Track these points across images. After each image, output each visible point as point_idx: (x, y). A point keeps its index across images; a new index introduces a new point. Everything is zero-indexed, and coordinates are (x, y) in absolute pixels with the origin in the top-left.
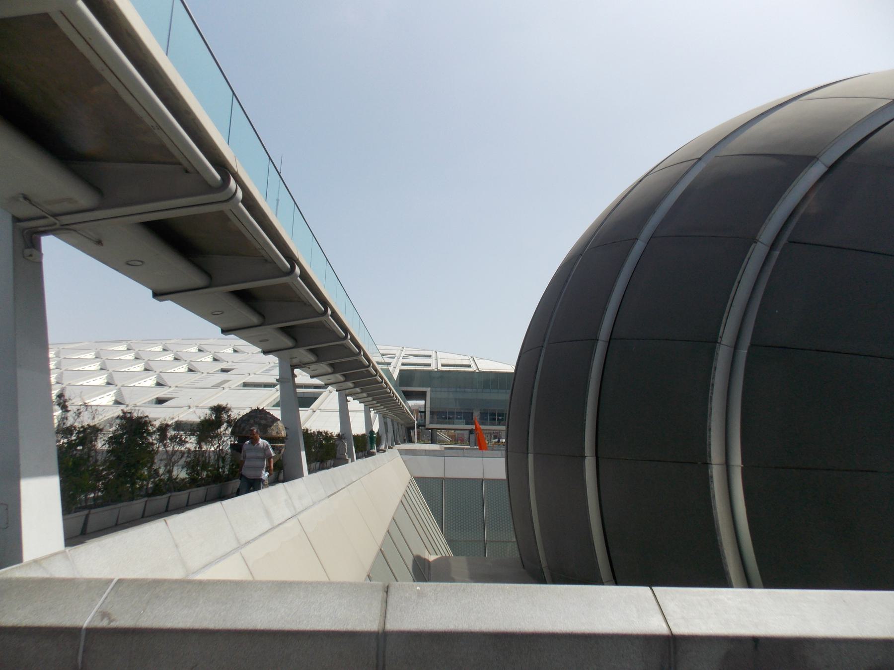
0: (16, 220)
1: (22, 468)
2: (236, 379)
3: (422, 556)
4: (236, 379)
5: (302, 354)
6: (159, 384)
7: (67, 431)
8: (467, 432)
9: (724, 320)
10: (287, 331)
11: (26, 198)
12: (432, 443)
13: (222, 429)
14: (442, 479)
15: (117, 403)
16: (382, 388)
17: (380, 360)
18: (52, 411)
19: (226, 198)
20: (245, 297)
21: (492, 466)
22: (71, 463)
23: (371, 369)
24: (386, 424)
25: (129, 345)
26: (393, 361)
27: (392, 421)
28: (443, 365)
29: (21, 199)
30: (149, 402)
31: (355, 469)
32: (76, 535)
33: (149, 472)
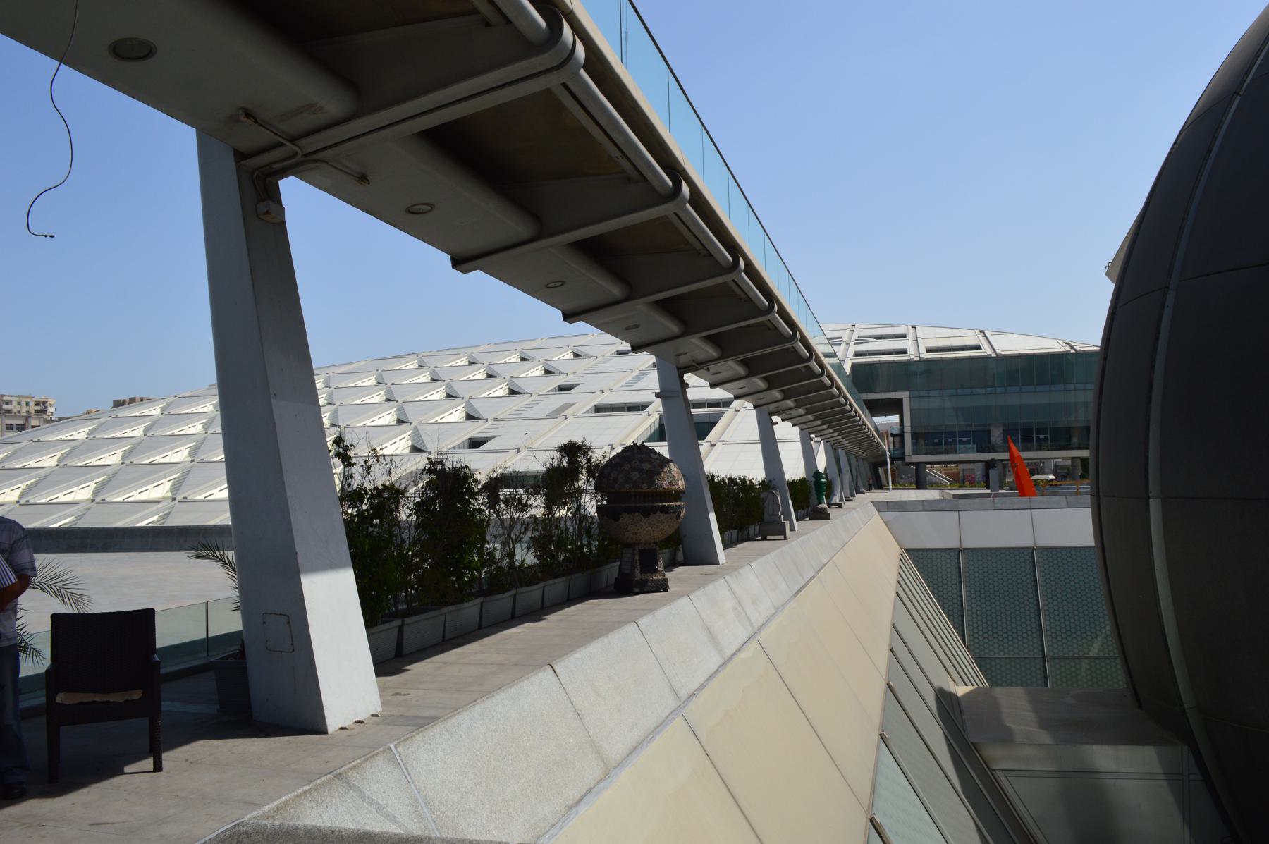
0: (240, 156)
1: (301, 559)
2: (583, 401)
3: (946, 688)
4: (583, 401)
5: (697, 346)
6: (470, 417)
7: (352, 496)
8: (979, 467)
10: (669, 307)
11: (248, 114)
12: (918, 488)
13: (581, 482)
14: (957, 552)
15: (415, 449)
16: (833, 396)
17: (828, 349)
18: (330, 468)
19: (558, 62)
20: (597, 252)
21: (1069, 525)
22: (367, 547)
23: (814, 365)
24: (837, 460)
25: (421, 360)
26: (840, 351)
27: (847, 453)
28: (929, 350)
29: (242, 118)
30: (459, 446)
31: (807, 538)
32: (389, 660)
33: (480, 557)
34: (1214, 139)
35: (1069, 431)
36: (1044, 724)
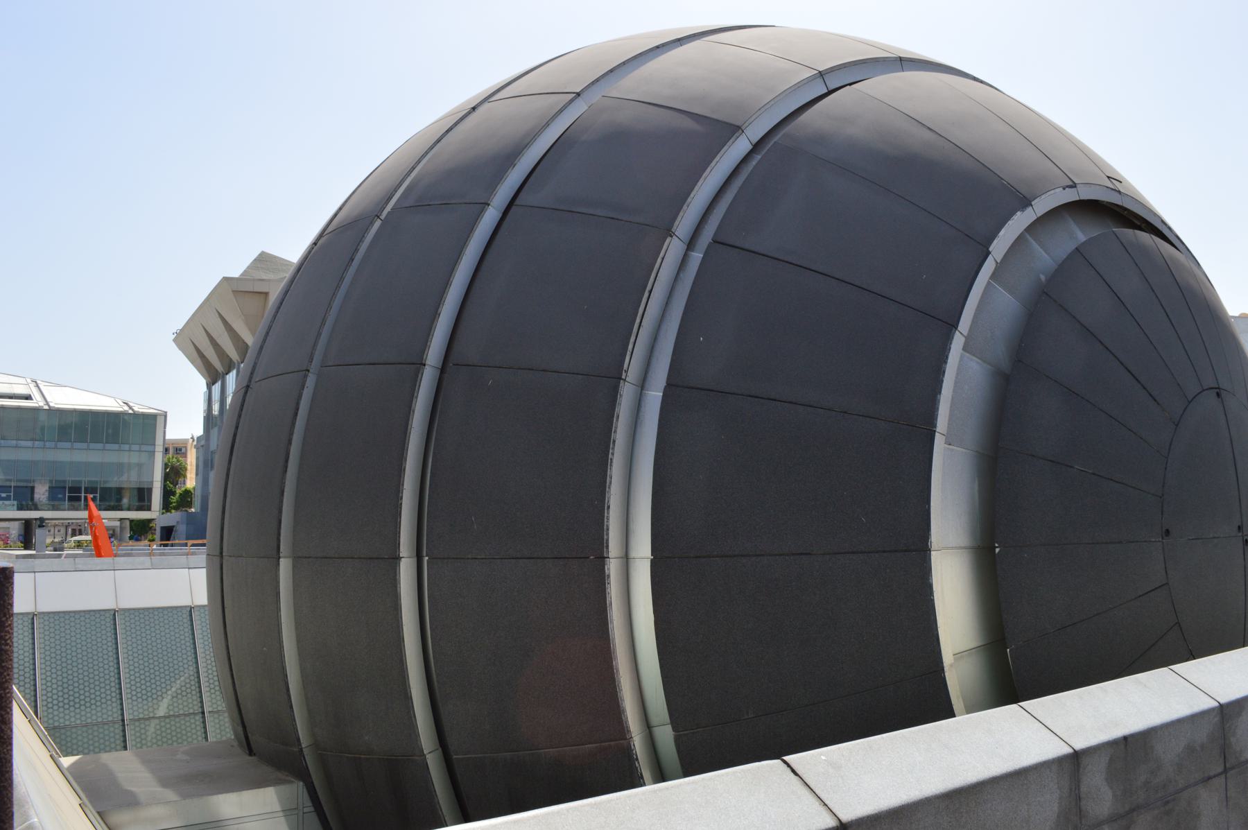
9: (630, 347)
34: (357, 250)
35: (119, 491)
36: (165, 782)
